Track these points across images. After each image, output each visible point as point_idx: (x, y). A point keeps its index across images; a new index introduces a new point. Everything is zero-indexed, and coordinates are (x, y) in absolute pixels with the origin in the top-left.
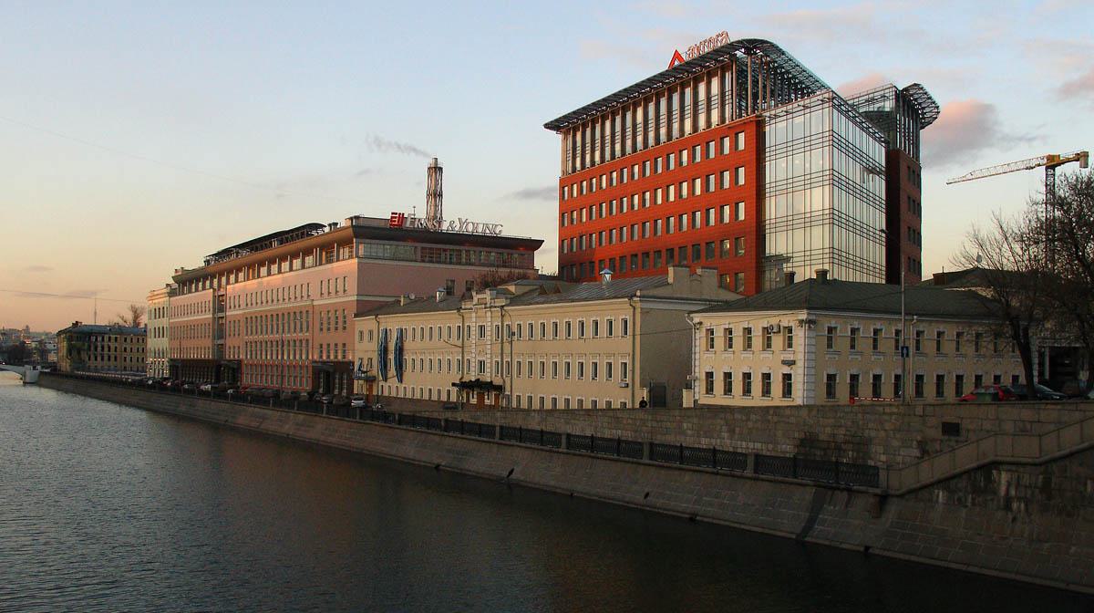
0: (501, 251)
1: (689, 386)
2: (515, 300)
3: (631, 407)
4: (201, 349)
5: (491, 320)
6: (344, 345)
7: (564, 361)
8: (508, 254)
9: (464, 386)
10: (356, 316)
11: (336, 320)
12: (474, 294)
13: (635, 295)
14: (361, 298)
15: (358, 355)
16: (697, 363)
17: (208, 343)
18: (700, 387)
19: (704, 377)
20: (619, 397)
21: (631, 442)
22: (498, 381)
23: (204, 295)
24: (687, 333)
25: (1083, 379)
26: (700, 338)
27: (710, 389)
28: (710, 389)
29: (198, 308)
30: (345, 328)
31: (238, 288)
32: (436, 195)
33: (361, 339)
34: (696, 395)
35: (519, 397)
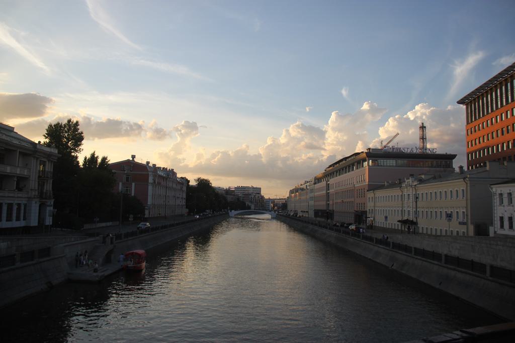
0: (446, 160)
1: (492, 224)
2: (421, 181)
3: (444, 234)
4: (322, 205)
5: (411, 192)
6: (364, 204)
7: (462, 211)
8: (445, 162)
9: (404, 222)
10: (368, 191)
11: (361, 193)
12: (406, 180)
13: (467, 177)
14: (370, 183)
15: (368, 208)
16: (495, 212)
17: (324, 203)
18: (497, 223)
19: (499, 218)
20: (455, 227)
21: (370, 259)
22: (415, 220)
23: (323, 184)
24: (490, 196)
25: (382, 235)
26: (496, 200)
27: (502, 226)
28: (502, 226)
29: (320, 189)
30: (364, 196)
31: (332, 181)
32: (423, 138)
33: (369, 201)
34: (495, 229)
35: (441, 230)
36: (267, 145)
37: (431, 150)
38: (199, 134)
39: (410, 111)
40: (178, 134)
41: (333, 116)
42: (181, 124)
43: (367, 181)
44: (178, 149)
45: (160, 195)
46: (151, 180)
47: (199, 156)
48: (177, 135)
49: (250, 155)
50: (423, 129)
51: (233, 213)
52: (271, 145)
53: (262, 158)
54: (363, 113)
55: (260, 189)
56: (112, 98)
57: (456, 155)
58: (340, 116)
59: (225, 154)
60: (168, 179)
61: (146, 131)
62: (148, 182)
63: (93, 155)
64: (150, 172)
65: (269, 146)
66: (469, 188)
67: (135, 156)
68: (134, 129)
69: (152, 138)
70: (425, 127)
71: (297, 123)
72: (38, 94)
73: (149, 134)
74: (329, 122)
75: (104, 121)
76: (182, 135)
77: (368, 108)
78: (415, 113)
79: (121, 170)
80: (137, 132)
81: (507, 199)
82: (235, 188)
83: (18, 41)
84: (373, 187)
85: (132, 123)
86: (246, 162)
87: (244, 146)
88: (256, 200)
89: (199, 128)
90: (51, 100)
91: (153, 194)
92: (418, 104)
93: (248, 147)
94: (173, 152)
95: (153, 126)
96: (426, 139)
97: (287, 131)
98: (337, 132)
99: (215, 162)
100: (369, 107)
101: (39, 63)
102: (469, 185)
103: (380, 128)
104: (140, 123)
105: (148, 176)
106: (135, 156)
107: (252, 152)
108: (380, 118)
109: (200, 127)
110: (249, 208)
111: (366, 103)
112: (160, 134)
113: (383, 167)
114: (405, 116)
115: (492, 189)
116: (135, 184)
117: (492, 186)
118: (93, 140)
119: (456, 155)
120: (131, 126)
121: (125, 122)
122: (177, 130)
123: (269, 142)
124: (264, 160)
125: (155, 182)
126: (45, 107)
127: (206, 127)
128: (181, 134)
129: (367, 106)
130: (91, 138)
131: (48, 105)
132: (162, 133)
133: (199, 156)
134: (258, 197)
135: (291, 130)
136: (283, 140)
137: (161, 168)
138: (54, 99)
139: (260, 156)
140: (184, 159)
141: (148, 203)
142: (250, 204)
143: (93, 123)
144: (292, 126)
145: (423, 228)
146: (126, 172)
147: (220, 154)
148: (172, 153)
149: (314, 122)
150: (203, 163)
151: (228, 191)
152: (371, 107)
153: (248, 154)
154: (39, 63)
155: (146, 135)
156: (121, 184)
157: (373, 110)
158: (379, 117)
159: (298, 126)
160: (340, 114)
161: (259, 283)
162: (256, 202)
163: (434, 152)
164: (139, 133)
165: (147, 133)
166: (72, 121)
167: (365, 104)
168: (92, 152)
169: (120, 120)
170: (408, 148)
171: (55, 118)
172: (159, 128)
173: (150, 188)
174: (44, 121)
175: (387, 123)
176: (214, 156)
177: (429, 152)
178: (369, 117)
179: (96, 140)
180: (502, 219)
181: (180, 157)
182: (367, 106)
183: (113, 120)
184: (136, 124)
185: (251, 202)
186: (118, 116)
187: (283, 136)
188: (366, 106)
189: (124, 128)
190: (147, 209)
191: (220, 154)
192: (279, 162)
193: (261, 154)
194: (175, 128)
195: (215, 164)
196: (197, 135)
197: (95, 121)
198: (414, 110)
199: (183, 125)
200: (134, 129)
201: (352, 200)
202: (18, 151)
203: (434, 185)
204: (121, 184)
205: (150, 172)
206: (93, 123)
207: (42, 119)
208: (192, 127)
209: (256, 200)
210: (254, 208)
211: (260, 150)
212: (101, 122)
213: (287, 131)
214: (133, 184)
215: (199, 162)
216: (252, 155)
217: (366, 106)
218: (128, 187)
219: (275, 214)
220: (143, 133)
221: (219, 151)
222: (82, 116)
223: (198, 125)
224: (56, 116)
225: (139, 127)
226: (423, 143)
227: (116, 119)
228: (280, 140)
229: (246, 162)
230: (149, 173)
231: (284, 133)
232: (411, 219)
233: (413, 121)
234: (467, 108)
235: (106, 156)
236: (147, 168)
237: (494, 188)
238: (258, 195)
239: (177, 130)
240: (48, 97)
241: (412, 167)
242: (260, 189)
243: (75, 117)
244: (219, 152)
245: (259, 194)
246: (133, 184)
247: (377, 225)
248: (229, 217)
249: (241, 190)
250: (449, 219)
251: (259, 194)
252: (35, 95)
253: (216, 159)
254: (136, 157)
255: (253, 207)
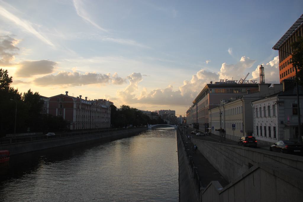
14: (210, 105)
36: (184, 85)
37: (253, 81)
38: (142, 80)
39: (271, 61)
40: (130, 81)
41: (223, 67)
42: (132, 74)
43: (209, 103)
44: (131, 89)
45: (99, 117)
46: (75, 106)
47: (143, 93)
48: (129, 81)
49: (173, 92)
50: (262, 69)
51: (151, 126)
52: (186, 85)
53: (181, 93)
54: (241, 63)
55: (175, 111)
56: (91, 61)
57: (271, 84)
58: (226, 66)
59: (158, 91)
60: (92, 106)
61: (111, 79)
62: (73, 107)
63: (29, 91)
64: (74, 101)
65: (185, 86)
66: (244, 104)
67: (68, 92)
68: (104, 79)
69: (115, 83)
70: (263, 68)
71: (201, 71)
72: (48, 61)
73: (113, 81)
74: (221, 70)
75: (87, 75)
76: (132, 81)
77: (244, 61)
78: (274, 62)
79: (57, 101)
80: (106, 80)
81: (272, 110)
82: (159, 111)
83: (37, 30)
84: (211, 107)
85: (103, 75)
86: (171, 96)
87: (169, 86)
88: (171, 118)
89: (142, 76)
90: (56, 63)
91: (77, 115)
92: (276, 57)
93: (172, 86)
94: (128, 91)
95: (115, 76)
96: (264, 75)
97: (195, 76)
98: (225, 76)
99: (153, 96)
100: (245, 59)
101: (49, 42)
102: (244, 103)
103: (252, 72)
104: (107, 75)
105: (73, 104)
106: (68, 92)
107: (175, 90)
108: (251, 66)
109: (143, 75)
110: (166, 123)
111: (242, 57)
112: (119, 81)
113: (219, 94)
114: (267, 64)
115: (253, 105)
116: (66, 110)
117: (253, 103)
118: (81, 85)
119: (271, 84)
120: (102, 77)
121: (98, 75)
122: (130, 78)
123: (185, 84)
124: (182, 94)
125: (78, 108)
126: (53, 68)
127: (146, 76)
128: (132, 80)
129: (244, 59)
130: (80, 85)
131: (54, 67)
132: (120, 80)
133: (143, 93)
134: (173, 116)
135: (198, 75)
136: (192, 82)
137: (103, 100)
138: (57, 62)
139: (179, 92)
140: (134, 95)
141: (74, 121)
142: (167, 121)
143: (80, 76)
144: (198, 73)
145: (236, 136)
146: (60, 102)
147: (156, 92)
148: (127, 91)
149: (213, 71)
150: (146, 97)
151: (153, 114)
152: (246, 60)
153: (172, 91)
154: (49, 42)
155: (111, 81)
156: (57, 109)
157: (247, 62)
158: (251, 65)
159: (202, 73)
160: (226, 64)
161: (99, 178)
162: (171, 119)
163: (256, 82)
164: (107, 81)
165: (112, 80)
166: (3, 70)
167: (242, 58)
168: (28, 90)
169: (96, 74)
170: (237, 81)
171: (58, 74)
172: (118, 77)
173: (75, 111)
174: (52, 76)
175: (256, 69)
176: (152, 93)
177: (252, 82)
178: (245, 66)
179: (83, 85)
180: (257, 127)
181: (132, 94)
182: (244, 59)
183: (92, 74)
184: (105, 76)
185: (168, 119)
186: (94, 72)
187: (192, 80)
188: (242, 59)
189: (99, 78)
190: (71, 125)
191: (156, 92)
192: (192, 95)
193: (180, 91)
194: (128, 77)
195: (153, 97)
196: (141, 81)
197: (81, 74)
198: (273, 60)
199: (132, 75)
200: (104, 79)
201: (204, 116)
202: (297, 108)
203: (233, 103)
204: (57, 109)
205: (74, 101)
206: (80, 76)
207: (52, 75)
208: (138, 76)
209: (171, 118)
210: (169, 123)
211: (180, 88)
212: (85, 75)
213: (195, 76)
214: (64, 109)
215: (143, 96)
216: (175, 91)
217: (242, 59)
218: (61, 111)
219: (177, 126)
220: (109, 80)
221: (155, 90)
222: (74, 72)
223: (142, 74)
224: (59, 73)
225: (107, 77)
226: (262, 78)
227: (93, 73)
228: (191, 82)
229: (171, 96)
230: (74, 102)
231: (193, 77)
232: (223, 129)
233: (273, 67)
234: (279, 52)
235: (37, 92)
236: (72, 99)
237: (254, 104)
238: (172, 115)
239: (130, 78)
240: (54, 61)
241: (231, 93)
242: (175, 111)
243: (70, 73)
244: (155, 91)
245: (173, 114)
246: (64, 109)
247: (212, 133)
248: (148, 129)
249: (163, 113)
250: (234, 128)
251: (173, 114)
252: (47, 61)
253: (154, 94)
254: (68, 92)
255: (168, 122)
